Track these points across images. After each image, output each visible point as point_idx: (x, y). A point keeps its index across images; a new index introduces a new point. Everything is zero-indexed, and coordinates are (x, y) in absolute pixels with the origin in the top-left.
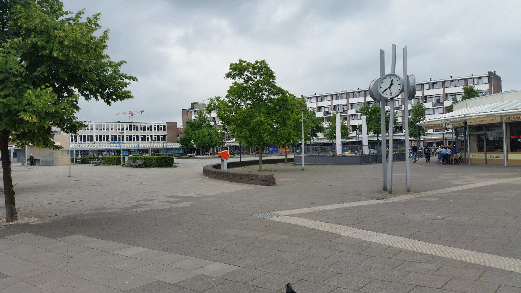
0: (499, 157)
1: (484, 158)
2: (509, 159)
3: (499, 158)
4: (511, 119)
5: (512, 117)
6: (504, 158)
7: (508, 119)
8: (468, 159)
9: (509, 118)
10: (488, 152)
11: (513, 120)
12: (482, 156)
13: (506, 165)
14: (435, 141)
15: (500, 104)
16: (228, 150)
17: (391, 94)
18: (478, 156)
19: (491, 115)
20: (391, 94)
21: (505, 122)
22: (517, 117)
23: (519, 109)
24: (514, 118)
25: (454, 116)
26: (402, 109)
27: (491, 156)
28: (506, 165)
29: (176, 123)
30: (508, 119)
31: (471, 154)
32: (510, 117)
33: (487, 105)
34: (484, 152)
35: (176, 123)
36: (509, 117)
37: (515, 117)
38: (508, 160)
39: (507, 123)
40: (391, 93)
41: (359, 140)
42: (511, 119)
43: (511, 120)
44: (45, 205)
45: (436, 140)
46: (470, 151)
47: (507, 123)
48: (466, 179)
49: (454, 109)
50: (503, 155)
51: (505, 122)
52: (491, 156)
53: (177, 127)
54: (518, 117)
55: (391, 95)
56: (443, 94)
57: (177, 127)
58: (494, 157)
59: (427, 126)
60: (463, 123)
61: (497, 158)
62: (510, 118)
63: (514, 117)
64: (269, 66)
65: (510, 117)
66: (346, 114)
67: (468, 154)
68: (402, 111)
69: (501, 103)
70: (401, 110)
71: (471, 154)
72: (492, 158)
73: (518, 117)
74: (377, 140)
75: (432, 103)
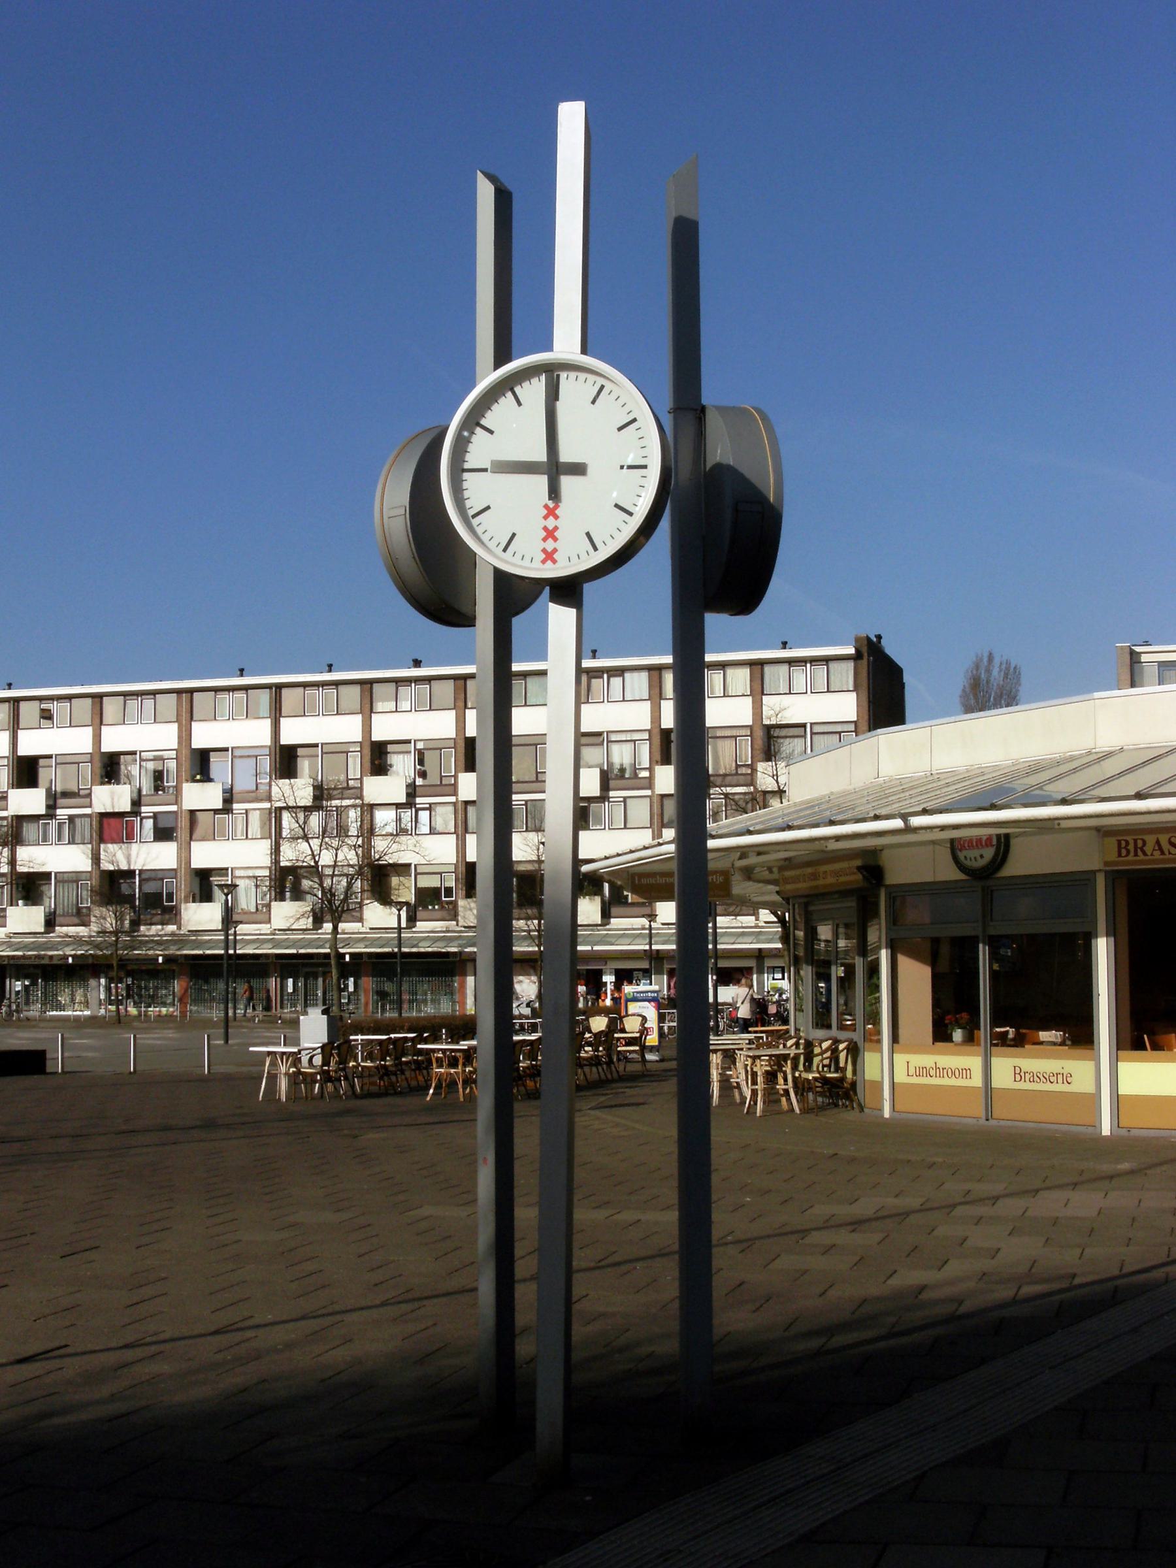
0: (1067, 1079)
1: (977, 1081)
2: (1123, 1090)
4: (1145, 854)
5: (1151, 840)
6: (882, 1078)
7: (1124, 852)
8: (878, 1085)
9: (1131, 847)
10: (1122, 1050)
12: (966, 1072)
15: (148, 1039)
17: (550, 545)
18: (940, 1071)
20: (550, 545)
21: (1106, 872)
24: (1161, 849)
26: (455, 794)
27: (1019, 1074)
30: (1124, 852)
31: (900, 1059)
32: (1135, 841)
33: (983, 765)
34: (979, 1045)
36: (1130, 839)
37: (1164, 839)
38: (1116, 1098)
39: (1114, 877)
40: (550, 534)
42: (1145, 854)
46: (895, 1039)
47: (1114, 877)
49: (1023, 690)
50: (878, 1055)
51: (1106, 872)
52: (1019, 1074)
55: (549, 556)
58: (1035, 1077)
59: (644, 881)
60: (859, 868)
62: (1140, 849)
63: (1158, 842)
65: (1140, 844)
66: (174, 808)
67: (877, 1055)
68: (455, 804)
69: (144, 1039)
70: (453, 799)
71: (900, 1059)
74: (327, 956)
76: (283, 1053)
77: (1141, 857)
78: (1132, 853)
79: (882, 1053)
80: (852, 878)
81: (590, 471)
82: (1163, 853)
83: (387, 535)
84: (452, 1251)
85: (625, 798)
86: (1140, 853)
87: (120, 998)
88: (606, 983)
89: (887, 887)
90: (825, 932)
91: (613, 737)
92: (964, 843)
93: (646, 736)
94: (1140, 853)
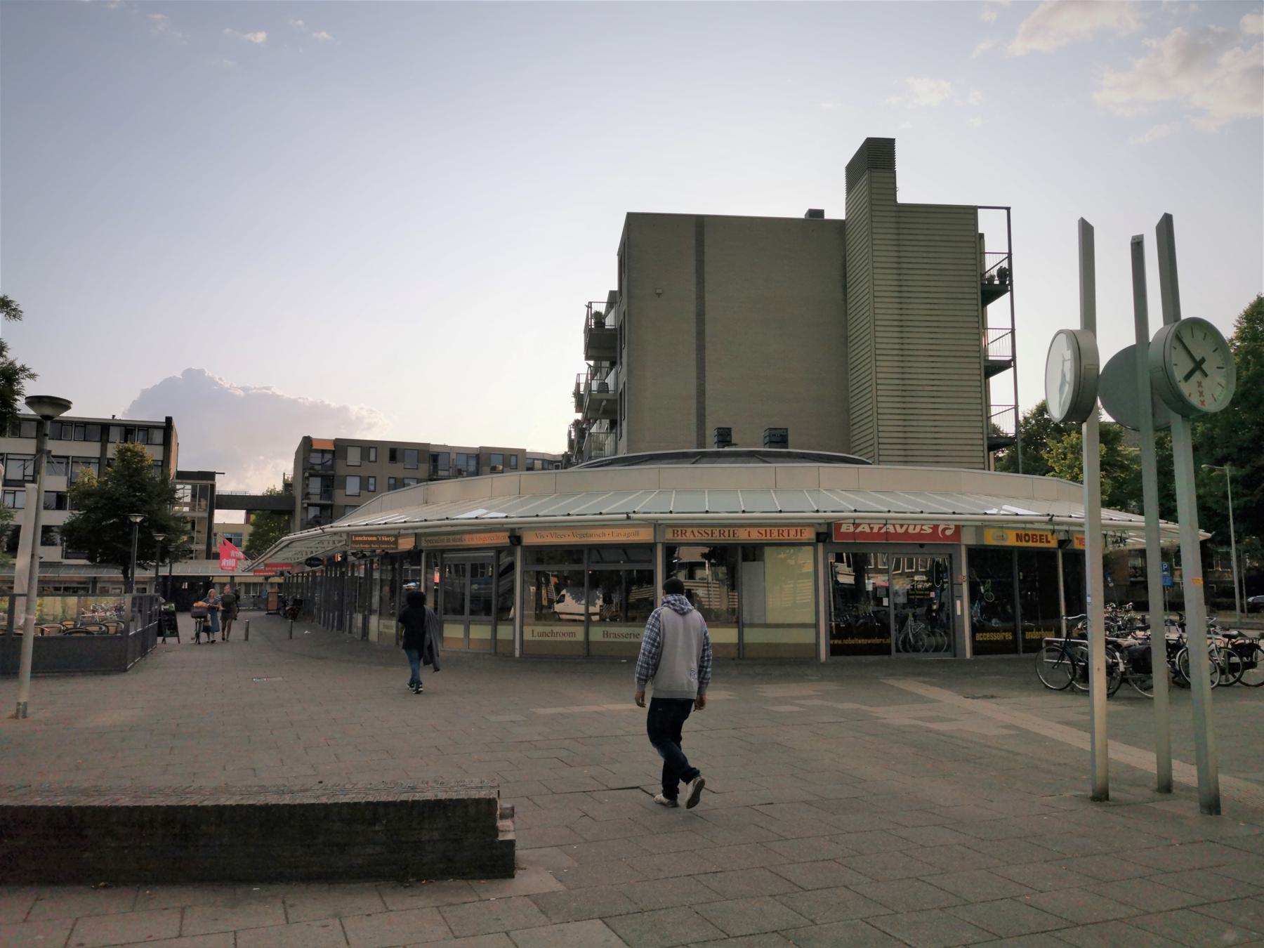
3: (573, 639)
4: (686, 536)
7: (676, 535)
9: (679, 533)
11: (691, 540)
13: (517, 654)
14: (62, 586)
16: (1024, 639)
19: (555, 524)
22: (700, 531)
23: (573, 515)
25: (707, 512)
28: (517, 654)
29: (893, 140)
35: (893, 140)
38: (522, 641)
41: (173, 574)
42: (686, 536)
43: (684, 540)
44: (890, 222)
45: (65, 582)
48: (885, 718)
50: (511, 628)
53: (902, 198)
54: (705, 532)
56: (162, 461)
57: (902, 198)
58: (615, 635)
61: (628, 640)
64: (897, 193)
72: (612, 639)
73: (705, 532)
75: (66, 478)
76: (1091, 713)
77: (722, 537)
78: (680, 535)
79: (514, 626)
80: (504, 541)
81: (24, 317)
82: (695, 536)
83: (1082, 379)
84: (947, 891)
85: (15, 491)
86: (781, 535)
87: (624, 860)
88: (596, 604)
89: (522, 546)
90: (361, 573)
91: (10, 457)
92: (176, 534)
93: (97, 461)
94: (781, 535)
